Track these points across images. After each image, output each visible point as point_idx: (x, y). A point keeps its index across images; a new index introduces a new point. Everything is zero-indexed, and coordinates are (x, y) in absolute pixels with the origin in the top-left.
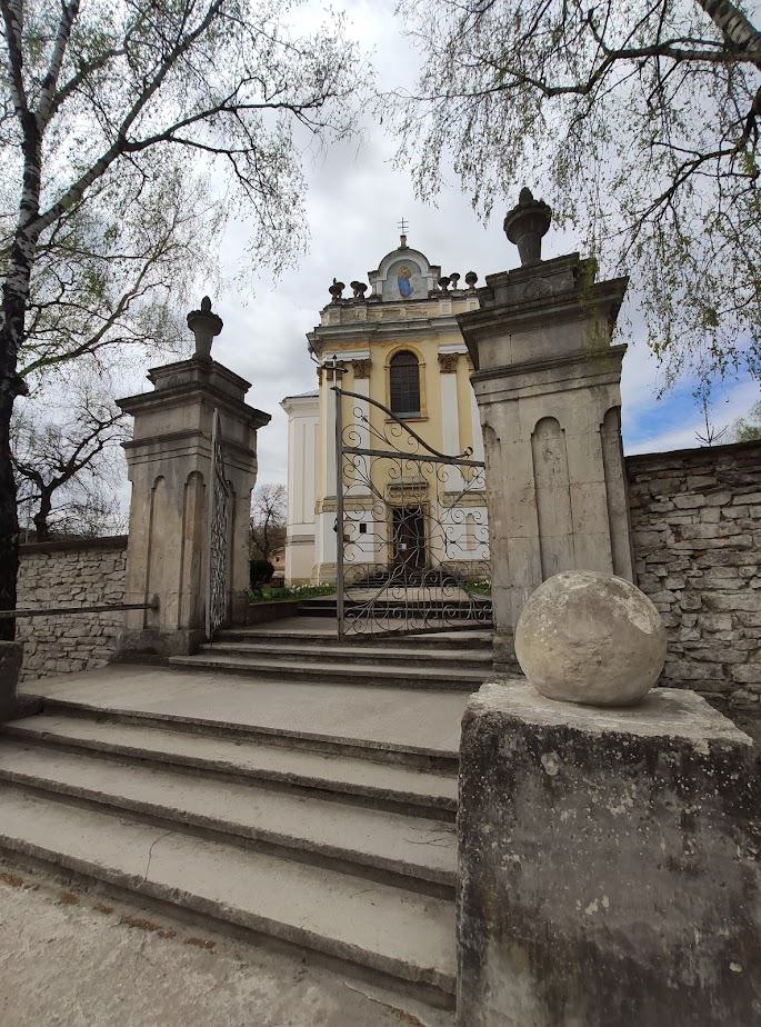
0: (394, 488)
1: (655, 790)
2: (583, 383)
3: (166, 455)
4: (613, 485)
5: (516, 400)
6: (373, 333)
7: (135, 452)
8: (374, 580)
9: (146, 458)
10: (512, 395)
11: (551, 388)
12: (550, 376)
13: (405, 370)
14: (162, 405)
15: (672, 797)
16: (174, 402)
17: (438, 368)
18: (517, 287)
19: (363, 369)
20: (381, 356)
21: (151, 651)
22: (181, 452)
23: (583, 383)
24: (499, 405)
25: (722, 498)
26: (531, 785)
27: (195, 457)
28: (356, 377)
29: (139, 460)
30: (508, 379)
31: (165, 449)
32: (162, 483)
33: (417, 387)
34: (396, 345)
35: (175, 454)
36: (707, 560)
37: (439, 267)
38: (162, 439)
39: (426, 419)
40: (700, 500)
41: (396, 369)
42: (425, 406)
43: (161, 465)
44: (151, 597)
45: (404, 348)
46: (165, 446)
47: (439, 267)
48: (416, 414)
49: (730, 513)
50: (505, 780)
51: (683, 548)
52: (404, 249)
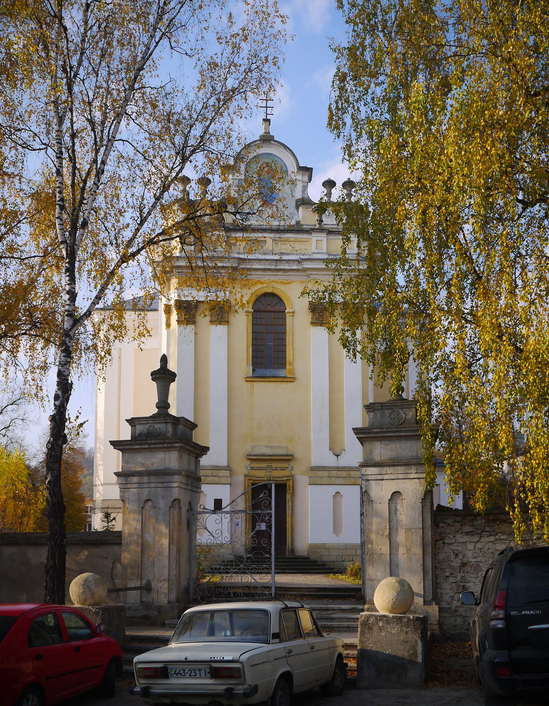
0: (254, 458)
1: (402, 627)
2: (416, 476)
3: (153, 485)
4: (426, 530)
5: (382, 480)
6: (235, 269)
7: (127, 480)
8: (236, 564)
9: (136, 486)
10: (380, 477)
11: (401, 476)
12: (401, 469)
13: (269, 315)
14: (149, 448)
15: (404, 628)
16: (160, 448)
17: (308, 317)
18: (386, 411)
19: (221, 313)
20: (243, 295)
21: (147, 617)
22: (165, 485)
23: (416, 476)
24: (373, 482)
25: (476, 538)
26: (376, 628)
27: (177, 489)
28: (212, 322)
29: (129, 486)
30: (378, 468)
31: (152, 481)
32: (150, 503)
33: (283, 340)
34: (259, 286)
35: (160, 485)
36: (468, 569)
37: (311, 169)
38: (150, 473)
39: (293, 379)
40: (466, 538)
41: (259, 314)
42: (291, 364)
43: (149, 491)
44: (144, 582)
45: (270, 290)
46: (153, 479)
47: (311, 169)
48: (281, 373)
49: (479, 545)
50: (370, 628)
51: (456, 563)
52: (267, 139)
